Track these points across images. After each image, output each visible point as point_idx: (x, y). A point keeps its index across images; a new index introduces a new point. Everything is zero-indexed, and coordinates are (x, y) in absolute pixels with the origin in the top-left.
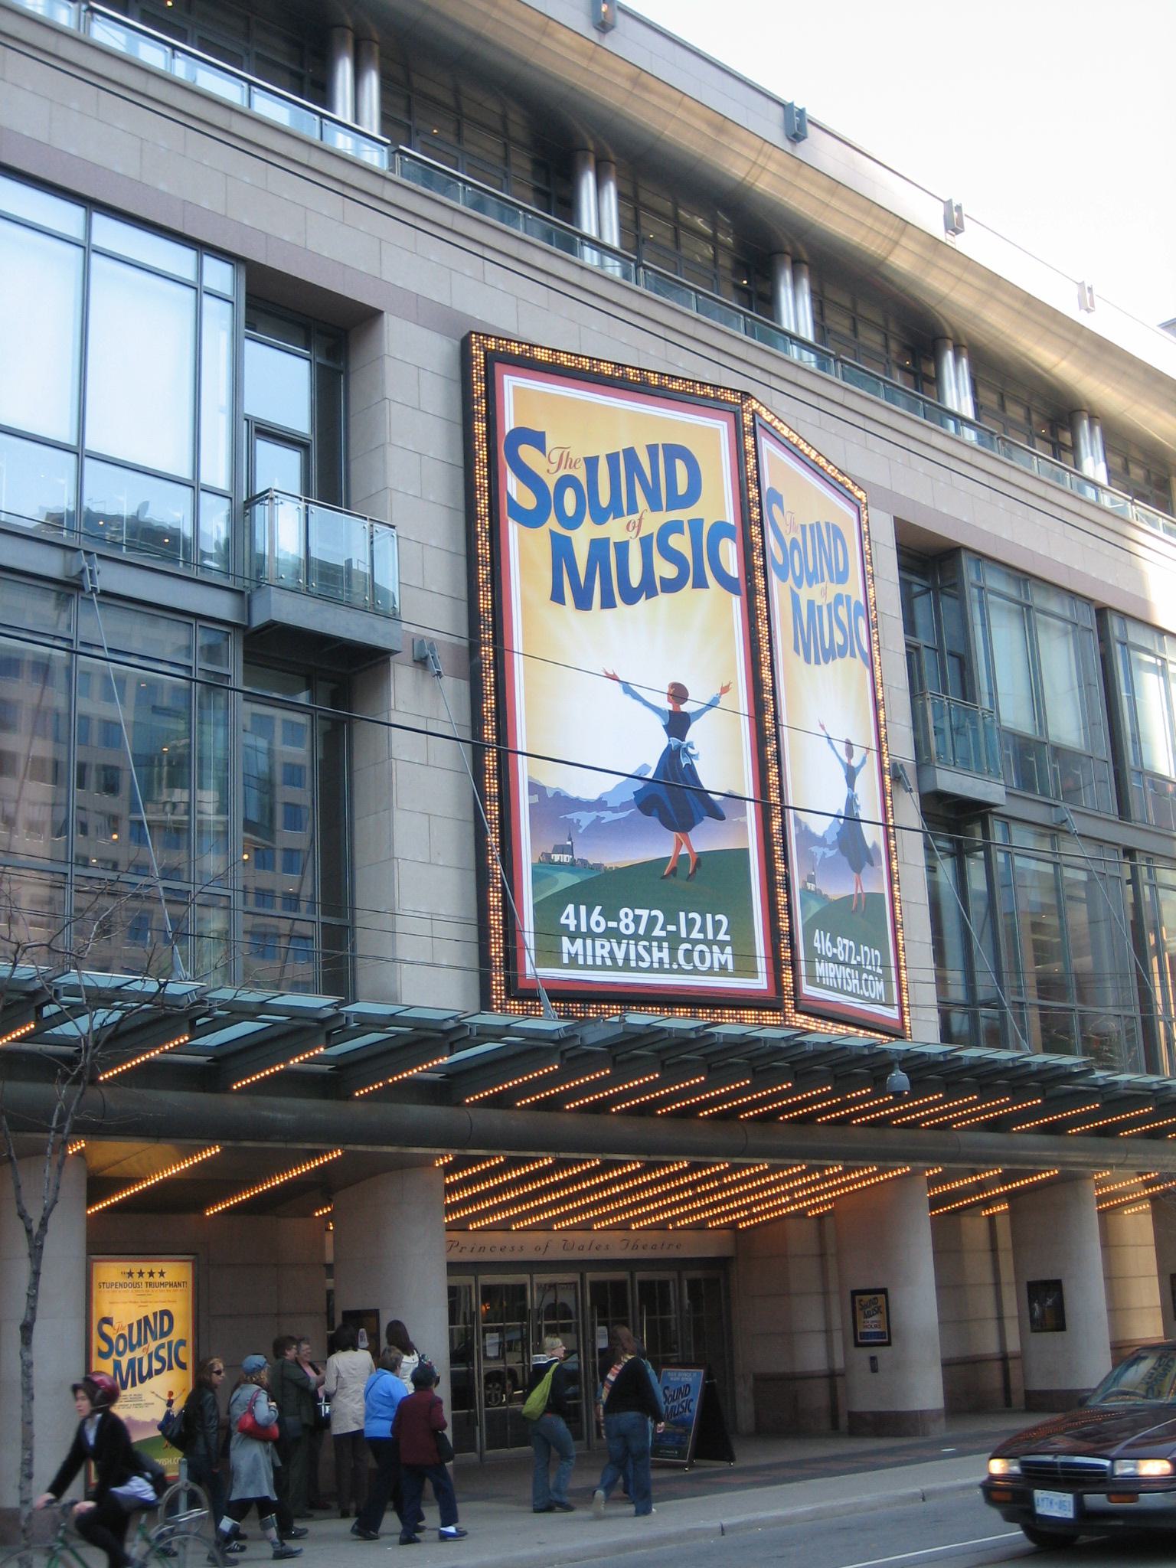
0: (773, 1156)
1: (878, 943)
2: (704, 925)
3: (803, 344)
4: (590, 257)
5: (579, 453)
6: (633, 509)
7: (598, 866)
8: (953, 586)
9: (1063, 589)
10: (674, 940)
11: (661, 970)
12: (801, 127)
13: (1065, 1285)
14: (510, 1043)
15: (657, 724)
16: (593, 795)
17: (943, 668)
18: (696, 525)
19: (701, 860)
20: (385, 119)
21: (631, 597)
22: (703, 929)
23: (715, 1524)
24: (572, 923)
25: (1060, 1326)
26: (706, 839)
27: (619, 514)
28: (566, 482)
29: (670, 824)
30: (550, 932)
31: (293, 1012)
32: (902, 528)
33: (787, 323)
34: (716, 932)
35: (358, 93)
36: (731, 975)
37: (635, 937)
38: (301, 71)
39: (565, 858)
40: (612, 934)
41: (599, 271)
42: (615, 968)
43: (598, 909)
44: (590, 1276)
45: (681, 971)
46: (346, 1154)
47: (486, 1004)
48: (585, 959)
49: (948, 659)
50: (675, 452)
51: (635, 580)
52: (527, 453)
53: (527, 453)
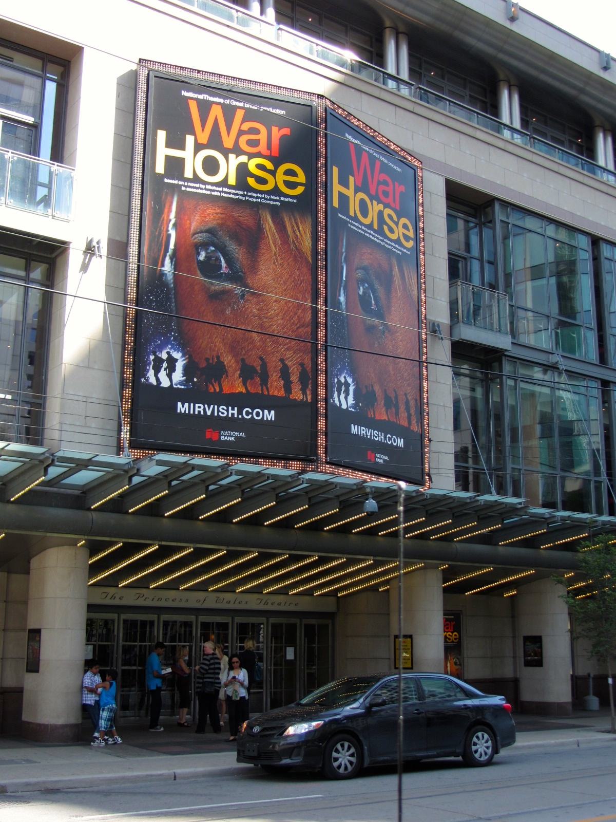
0: (496, 564)
4: (507, 134)
8: (490, 222)
12: (607, 63)
13: (544, 640)
20: (411, 70)
25: (539, 663)
32: (450, 184)
38: (527, 119)
41: (511, 141)
44: (272, 620)
46: (195, 549)
48: (378, 458)
49: (486, 266)
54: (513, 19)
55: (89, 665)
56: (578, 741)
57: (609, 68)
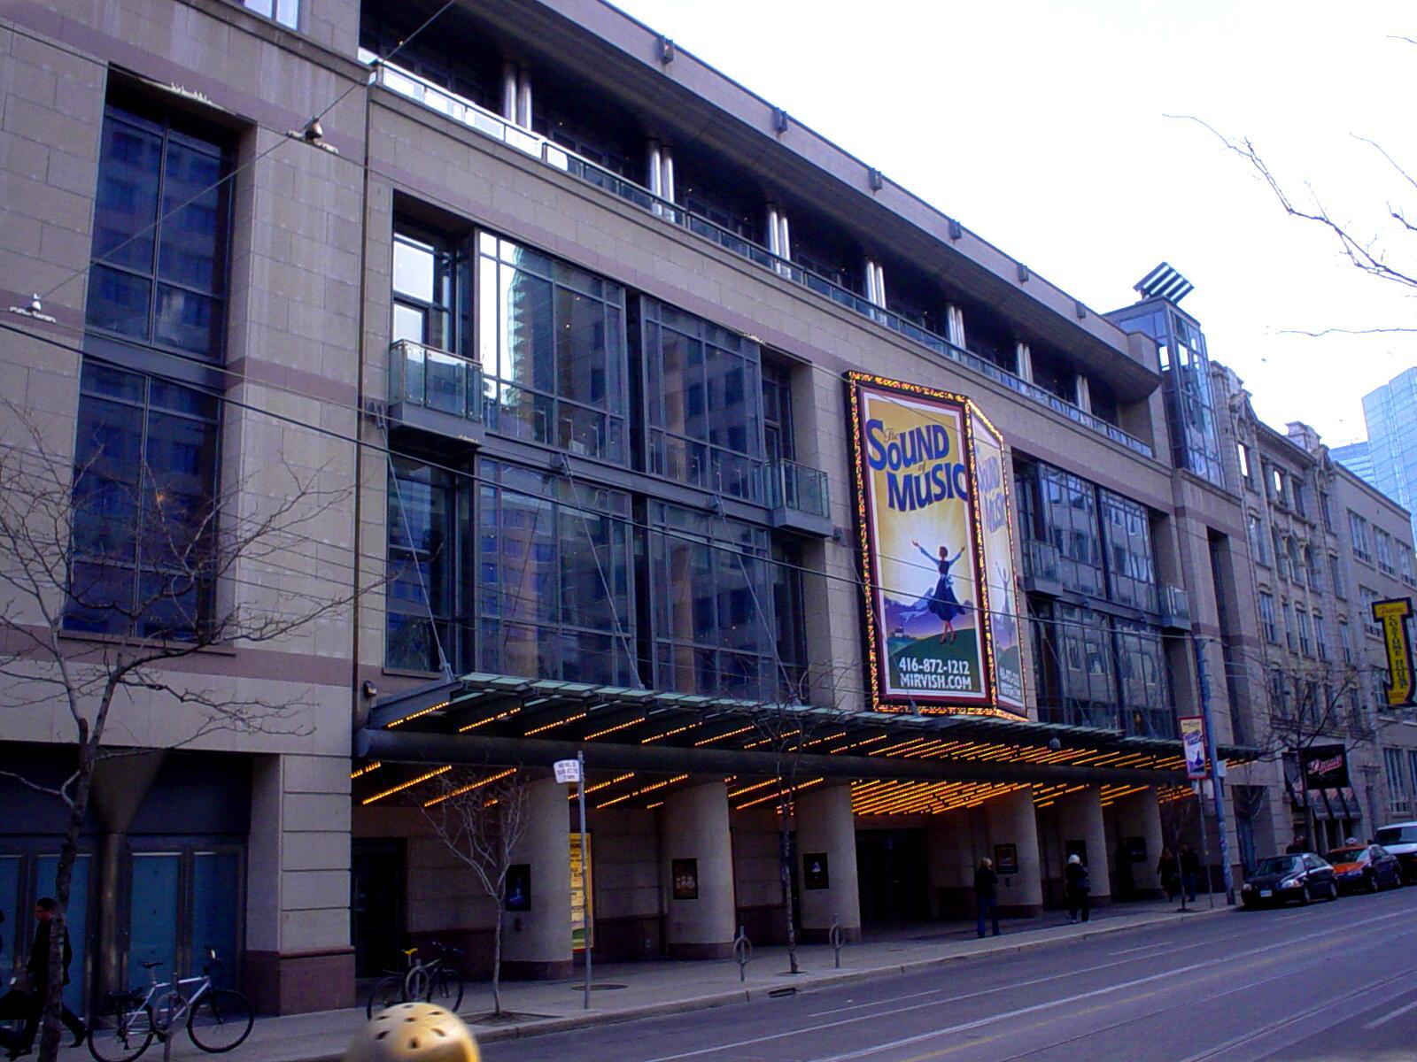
1: (1018, 672)
2: (959, 666)
3: (784, 262)
5: (897, 432)
6: (921, 459)
7: (914, 639)
9: (555, 257)
10: (946, 674)
11: (942, 689)
12: (784, 123)
13: (699, 862)
14: (486, 694)
15: (936, 567)
16: (910, 604)
17: (1034, 525)
18: (948, 466)
19: (956, 634)
21: (922, 505)
22: (958, 669)
23: (898, 966)
24: (904, 667)
26: (958, 625)
27: (915, 462)
28: (893, 446)
29: (943, 617)
30: (896, 674)
31: (501, 688)
32: (398, 195)
33: (873, 299)
34: (964, 669)
35: (520, 100)
36: (971, 691)
37: (931, 673)
39: (900, 635)
40: (921, 672)
42: (922, 688)
43: (915, 660)
45: (949, 689)
47: (869, 706)
50: (938, 429)
51: (923, 495)
52: (875, 431)
53: (875, 431)
54: (875, 188)
55: (1087, 874)
56: (586, 1007)
57: (786, 129)
